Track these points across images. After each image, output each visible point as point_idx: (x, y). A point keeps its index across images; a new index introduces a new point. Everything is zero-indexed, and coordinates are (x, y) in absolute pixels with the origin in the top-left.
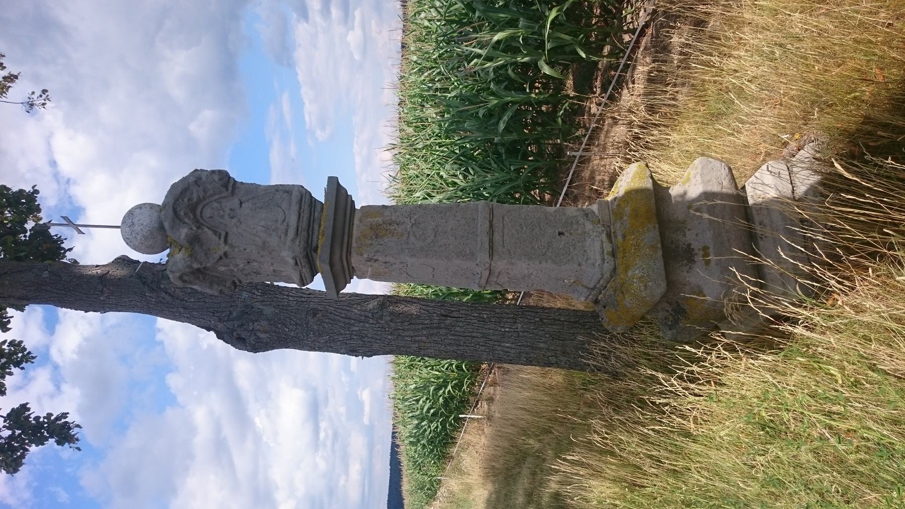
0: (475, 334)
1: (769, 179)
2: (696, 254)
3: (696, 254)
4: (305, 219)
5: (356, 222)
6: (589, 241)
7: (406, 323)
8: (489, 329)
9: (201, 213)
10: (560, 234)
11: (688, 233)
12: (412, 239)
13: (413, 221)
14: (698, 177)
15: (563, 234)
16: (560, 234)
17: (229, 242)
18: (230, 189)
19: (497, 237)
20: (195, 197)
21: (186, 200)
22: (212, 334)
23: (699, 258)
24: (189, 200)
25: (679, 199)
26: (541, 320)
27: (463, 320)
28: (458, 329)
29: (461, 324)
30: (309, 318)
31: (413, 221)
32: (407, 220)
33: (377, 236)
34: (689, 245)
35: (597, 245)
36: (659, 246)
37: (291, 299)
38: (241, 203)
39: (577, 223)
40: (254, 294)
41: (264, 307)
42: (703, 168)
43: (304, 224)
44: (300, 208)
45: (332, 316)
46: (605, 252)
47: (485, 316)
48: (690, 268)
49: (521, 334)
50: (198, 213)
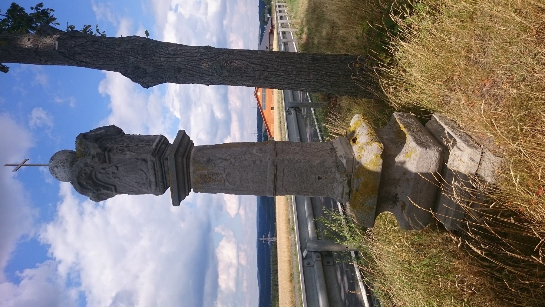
0: (282, 83)
1: (465, 158)
2: (399, 201)
3: (399, 201)
4: (159, 175)
5: (191, 175)
6: (336, 184)
7: (238, 77)
8: (291, 80)
9: (95, 176)
10: (319, 178)
11: (398, 188)
12: (227, 183)
13: (226, 173)
14: (415, 162)
15: (321, 178)
16: (319, 178)
17: (118, 190)
18: (108, 161)
19: (279, 182)
20: (88, 171)
21: (83, 175)
22: (120, 74)
23: (399, 204)
24: (85, 174)
25: (399, 165)
26: (326, 73)
27: (275, 73)
28: (272, 79)
29: (274, 76)
30: (177, 74)
31: (226, 173)
32: (223, 172)
33: (205, 182)
34: (397, 194)
35: (340, 189)
36: (375, 207)
37: (162, 59)
38: (117, 168)
39: (331, 171)
40: (138, 58)
41: (146, 67)
42: (420, 157)
43: (160, 179)
44: (155, 171)
45: (191, 72)
46: (345, 193)
47: (290, 70)
48: (393, 207)
49: (312, 83)
50: (94, 177)
